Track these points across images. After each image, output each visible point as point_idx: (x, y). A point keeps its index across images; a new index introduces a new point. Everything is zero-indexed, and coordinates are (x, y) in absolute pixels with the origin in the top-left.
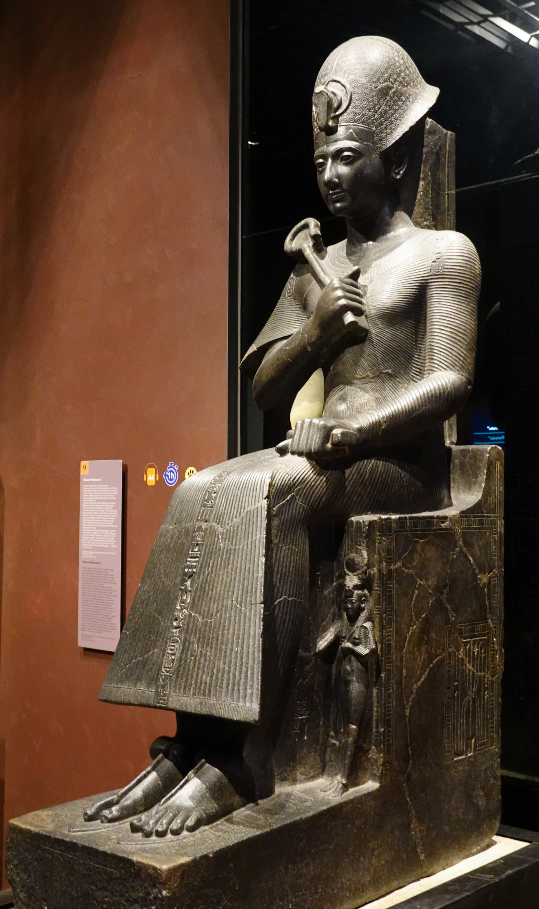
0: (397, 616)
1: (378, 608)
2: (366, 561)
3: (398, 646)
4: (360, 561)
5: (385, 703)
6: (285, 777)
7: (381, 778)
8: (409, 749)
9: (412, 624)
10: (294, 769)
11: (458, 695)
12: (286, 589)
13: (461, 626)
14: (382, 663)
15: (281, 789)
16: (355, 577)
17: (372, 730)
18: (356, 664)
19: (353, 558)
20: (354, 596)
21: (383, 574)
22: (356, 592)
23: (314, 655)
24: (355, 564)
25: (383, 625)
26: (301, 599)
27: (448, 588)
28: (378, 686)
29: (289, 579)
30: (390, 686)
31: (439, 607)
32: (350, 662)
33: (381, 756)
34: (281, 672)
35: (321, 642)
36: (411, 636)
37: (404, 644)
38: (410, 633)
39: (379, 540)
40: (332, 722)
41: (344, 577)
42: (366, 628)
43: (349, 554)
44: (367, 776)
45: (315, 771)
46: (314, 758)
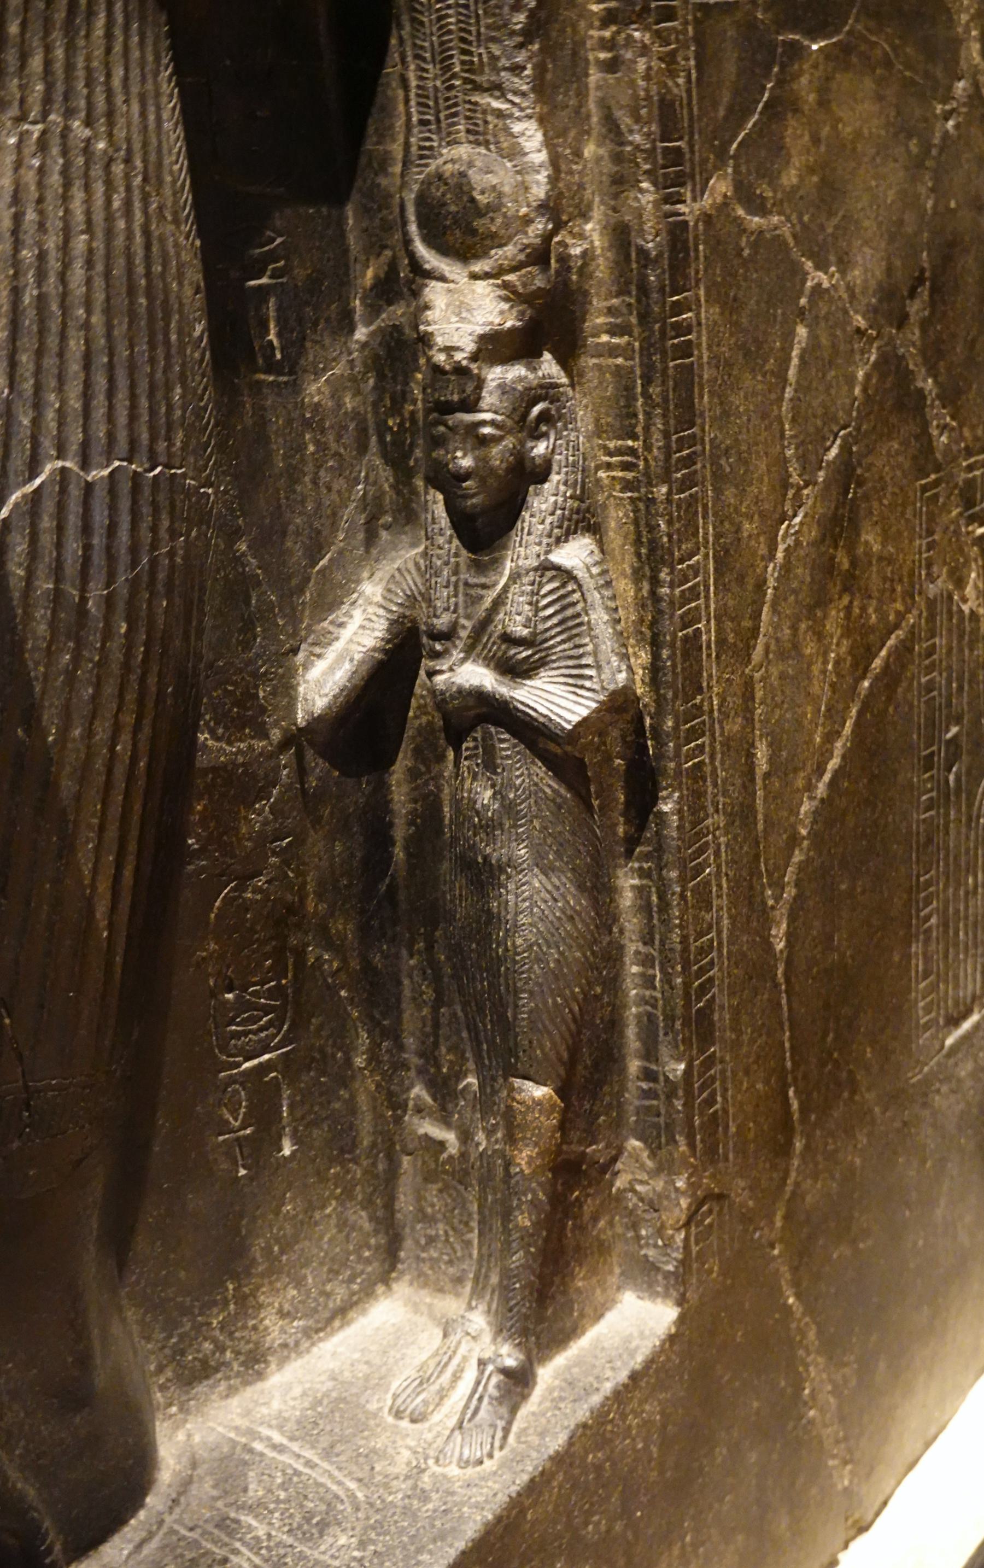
0: (719, 478)
1: (619, 452)
2: (539, 188)
3: (731, 638)
4: (507, 189)
5: (684, 939)
6: (204, 1362)
7: (678, 1284)
8: (791, 1093)
9: (788, 507)
10: (247, 1304)
11: (958, 779)
12: (61, 414)
13: (970, 468)
14: (660, 744)
15: (185, 1437)
16: (482, 287)
17: (623, 1070)
18: (527, 775)
19: (463, 175)
20: (489, 398)
21: (642, 252)
22: (495, 375)
23: (284, 745)
24: (480, 212)
25: (654, 545)
26: (168, 466)
27: (924, 292)
28: (646, 857)
29: (76, 345)
30: (701, 851)
31: (895, 399)
32: (490, 765)
33: (680, 1184)
34: (101, 910)
35: (317, 670)
36: (787, 568)
37: (757, 616)
38: (780, 555)
39: (605, 45)
40: (410, 1042)
41: (416, 294)
42: (566, 575)
43: (428, 152)
44: (613, 1280)
45: (351, 1280)
46: (343, 1224)
